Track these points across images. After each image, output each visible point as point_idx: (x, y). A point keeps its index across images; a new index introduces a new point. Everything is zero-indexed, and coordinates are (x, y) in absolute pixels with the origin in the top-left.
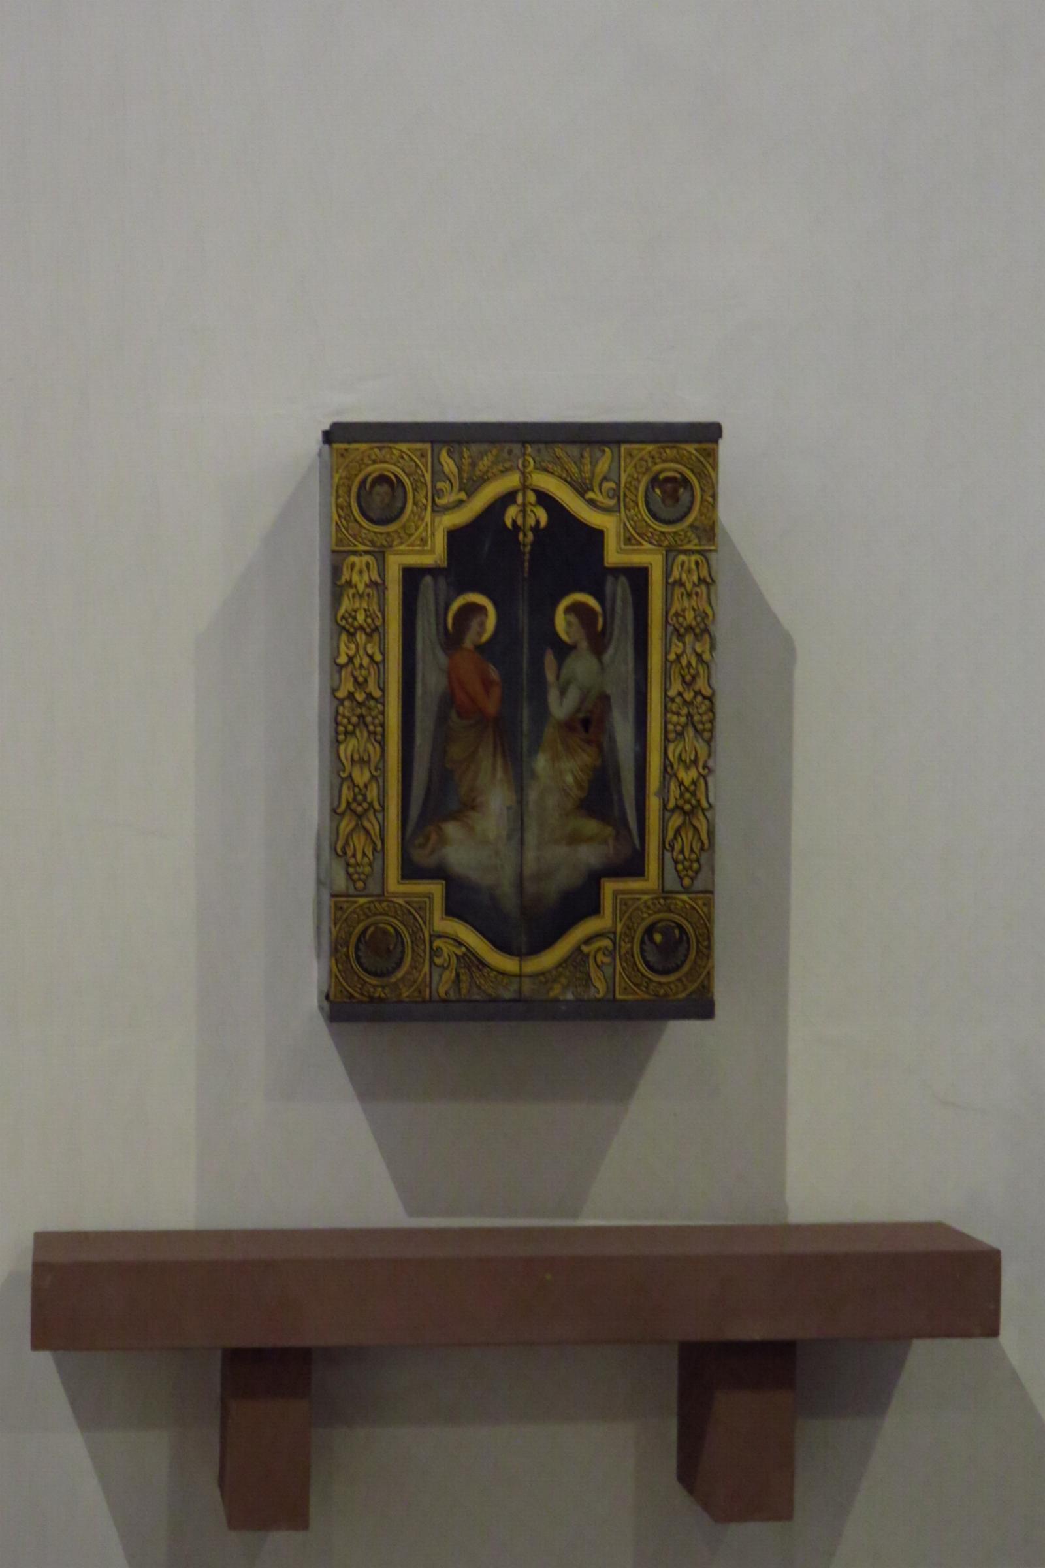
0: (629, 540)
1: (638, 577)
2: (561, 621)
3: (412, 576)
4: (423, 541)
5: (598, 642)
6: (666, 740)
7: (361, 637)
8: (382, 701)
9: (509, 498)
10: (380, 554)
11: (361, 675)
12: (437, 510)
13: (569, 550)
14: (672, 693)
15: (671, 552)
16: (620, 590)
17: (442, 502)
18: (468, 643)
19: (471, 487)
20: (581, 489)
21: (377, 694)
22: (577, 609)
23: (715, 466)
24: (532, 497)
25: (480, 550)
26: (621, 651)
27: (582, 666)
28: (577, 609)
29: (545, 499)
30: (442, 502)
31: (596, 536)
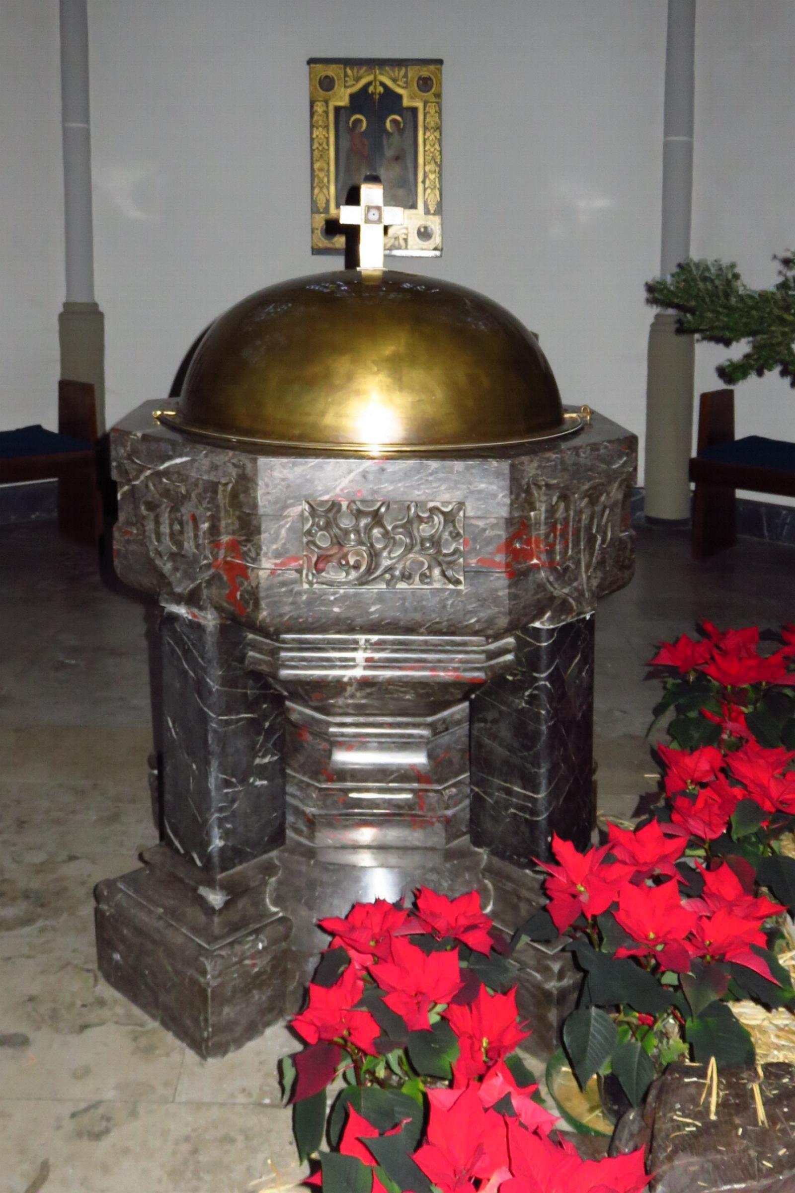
0: (411, 98)
1: (414, 110)
2: (388, 125)
3: (337, 109)
4: (341, 98)
5: (401, 131)
6: (425, 165)
7: (320, 129)
8: (328, 150)
9: (369, 84)
10: (326, 102)
11: (321, 141)
12: (346, 87)
13: (391, 100)
14: (314, 147)
15: (426, 103)
16: (409, 115)
17: (347, 84)
18: (357, 132)
19: (357, 79)
20: (394, 80)
21: (326, 147)
22: (394, 122)
23: (441, 74)
24: (378, 83)
25: (360, 101)
26: (409, 133)
27: (396, 139)
28: (394, 122)
29: (382, 84)
30: (347, 84)
31: (400, 97)
